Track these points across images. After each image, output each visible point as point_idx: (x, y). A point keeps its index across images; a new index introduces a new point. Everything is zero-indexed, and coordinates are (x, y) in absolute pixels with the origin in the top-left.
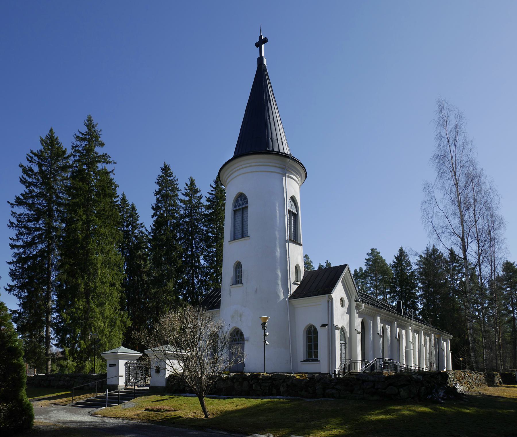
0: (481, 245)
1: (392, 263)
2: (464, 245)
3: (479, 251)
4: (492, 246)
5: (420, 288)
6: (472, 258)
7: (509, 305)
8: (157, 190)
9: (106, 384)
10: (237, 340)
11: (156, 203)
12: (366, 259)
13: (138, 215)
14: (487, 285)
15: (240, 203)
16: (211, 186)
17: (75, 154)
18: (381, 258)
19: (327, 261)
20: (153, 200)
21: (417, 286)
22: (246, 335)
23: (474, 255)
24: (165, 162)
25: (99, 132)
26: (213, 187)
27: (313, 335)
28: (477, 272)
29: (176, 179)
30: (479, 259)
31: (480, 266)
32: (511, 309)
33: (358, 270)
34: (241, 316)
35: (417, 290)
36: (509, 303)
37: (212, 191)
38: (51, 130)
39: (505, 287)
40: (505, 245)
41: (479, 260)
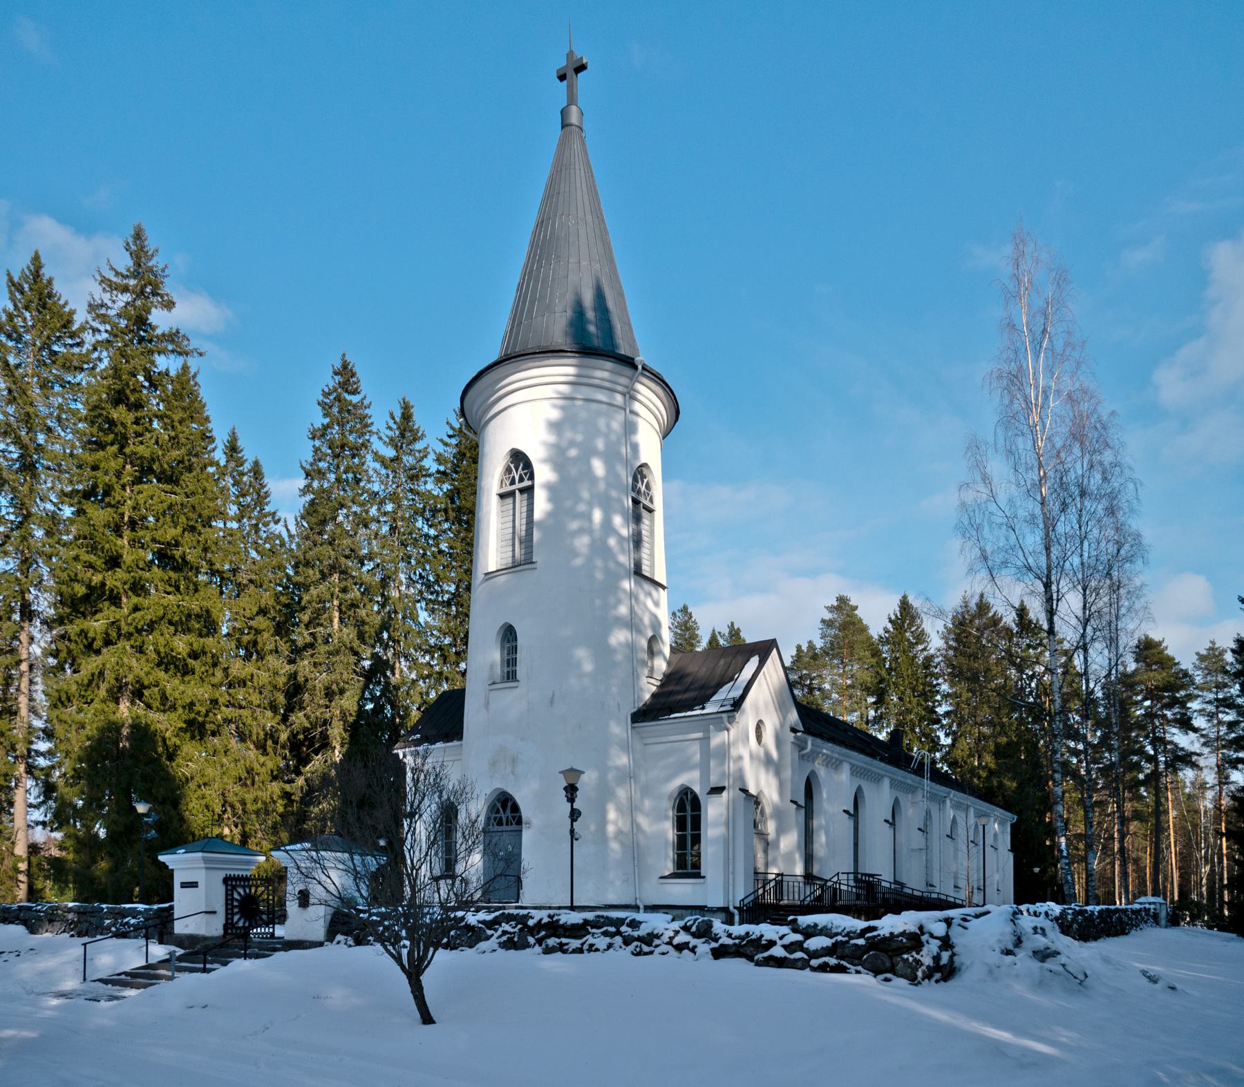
0: (1090, 600)
1: (882, 632)
2: (1049, 600)
3: (1084, 613)
4: (1115, 604)
5: (946, 696)
6: (1068, 632)
7: (1146, 743)
8: (318, 425)
9: (173, 933)
10: (504, 821)
11: (311, 460)
12: (823, 621)
13: (265, 490)
14: (1100, 695)
15: (514, 477)
16: (448, 423)
17: (96, 324)
18: (860, 621)
19: (732, 624)
20: (305, 451)
21: (938, 692)
22: (525, 813)
23: (1074, 621)
24: (344, 355)
25: (163, 270)
26: (452, 428)
27: (689, 813)
28: (1078, 662)
29: (366, 402)
30: (1085, 630)
31: (1085, 650)
32: (1152, 752)
33: (804, 648)
34: (514, 761)
35: (938, 701)
36: (1147, 737)
37: (450, 437)
38: (36, 259)
39: (1139, 698)
40: (1142, 600)
41: (1083, 636)
